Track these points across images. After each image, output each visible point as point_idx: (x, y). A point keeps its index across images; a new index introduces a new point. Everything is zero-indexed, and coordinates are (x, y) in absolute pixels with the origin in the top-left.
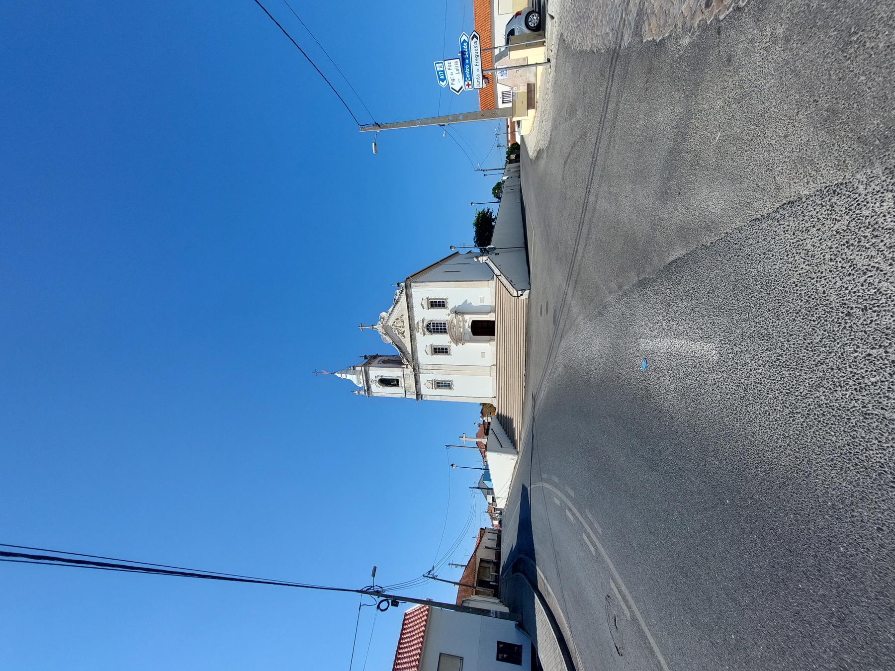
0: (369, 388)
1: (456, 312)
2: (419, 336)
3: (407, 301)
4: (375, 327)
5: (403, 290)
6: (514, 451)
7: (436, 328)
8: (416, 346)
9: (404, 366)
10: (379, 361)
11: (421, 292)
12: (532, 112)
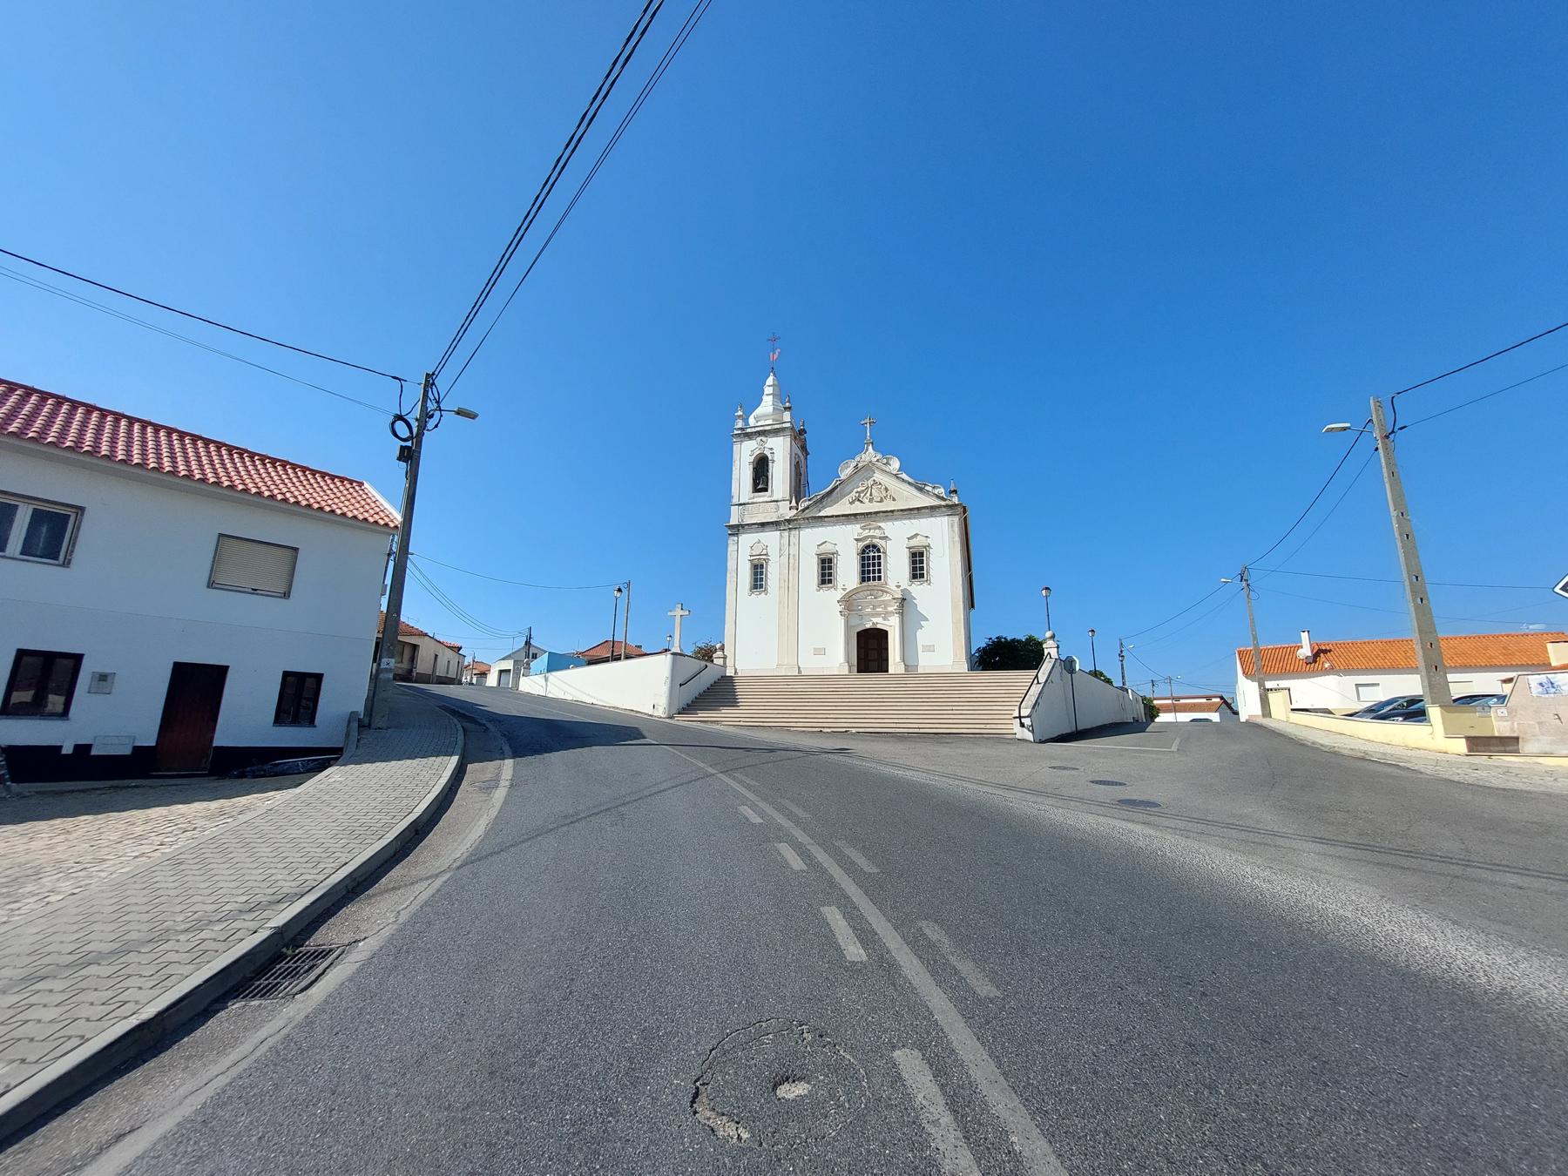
0: (749, 436)
1: (904, 599)
2: (855, 530)
3: (924, 508)
4: (870, 447)
5: (944, 500)
6: (677, 706)
7: (870, 562)
8: (835, 524)
9: (794, 501)
10: (799, 457)
11: (941, 535)
12: (1460, 746)
